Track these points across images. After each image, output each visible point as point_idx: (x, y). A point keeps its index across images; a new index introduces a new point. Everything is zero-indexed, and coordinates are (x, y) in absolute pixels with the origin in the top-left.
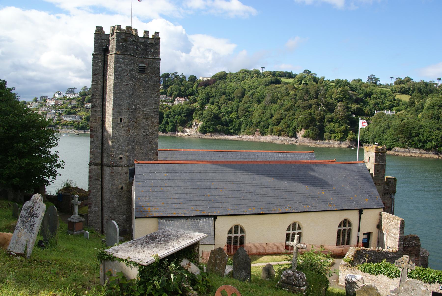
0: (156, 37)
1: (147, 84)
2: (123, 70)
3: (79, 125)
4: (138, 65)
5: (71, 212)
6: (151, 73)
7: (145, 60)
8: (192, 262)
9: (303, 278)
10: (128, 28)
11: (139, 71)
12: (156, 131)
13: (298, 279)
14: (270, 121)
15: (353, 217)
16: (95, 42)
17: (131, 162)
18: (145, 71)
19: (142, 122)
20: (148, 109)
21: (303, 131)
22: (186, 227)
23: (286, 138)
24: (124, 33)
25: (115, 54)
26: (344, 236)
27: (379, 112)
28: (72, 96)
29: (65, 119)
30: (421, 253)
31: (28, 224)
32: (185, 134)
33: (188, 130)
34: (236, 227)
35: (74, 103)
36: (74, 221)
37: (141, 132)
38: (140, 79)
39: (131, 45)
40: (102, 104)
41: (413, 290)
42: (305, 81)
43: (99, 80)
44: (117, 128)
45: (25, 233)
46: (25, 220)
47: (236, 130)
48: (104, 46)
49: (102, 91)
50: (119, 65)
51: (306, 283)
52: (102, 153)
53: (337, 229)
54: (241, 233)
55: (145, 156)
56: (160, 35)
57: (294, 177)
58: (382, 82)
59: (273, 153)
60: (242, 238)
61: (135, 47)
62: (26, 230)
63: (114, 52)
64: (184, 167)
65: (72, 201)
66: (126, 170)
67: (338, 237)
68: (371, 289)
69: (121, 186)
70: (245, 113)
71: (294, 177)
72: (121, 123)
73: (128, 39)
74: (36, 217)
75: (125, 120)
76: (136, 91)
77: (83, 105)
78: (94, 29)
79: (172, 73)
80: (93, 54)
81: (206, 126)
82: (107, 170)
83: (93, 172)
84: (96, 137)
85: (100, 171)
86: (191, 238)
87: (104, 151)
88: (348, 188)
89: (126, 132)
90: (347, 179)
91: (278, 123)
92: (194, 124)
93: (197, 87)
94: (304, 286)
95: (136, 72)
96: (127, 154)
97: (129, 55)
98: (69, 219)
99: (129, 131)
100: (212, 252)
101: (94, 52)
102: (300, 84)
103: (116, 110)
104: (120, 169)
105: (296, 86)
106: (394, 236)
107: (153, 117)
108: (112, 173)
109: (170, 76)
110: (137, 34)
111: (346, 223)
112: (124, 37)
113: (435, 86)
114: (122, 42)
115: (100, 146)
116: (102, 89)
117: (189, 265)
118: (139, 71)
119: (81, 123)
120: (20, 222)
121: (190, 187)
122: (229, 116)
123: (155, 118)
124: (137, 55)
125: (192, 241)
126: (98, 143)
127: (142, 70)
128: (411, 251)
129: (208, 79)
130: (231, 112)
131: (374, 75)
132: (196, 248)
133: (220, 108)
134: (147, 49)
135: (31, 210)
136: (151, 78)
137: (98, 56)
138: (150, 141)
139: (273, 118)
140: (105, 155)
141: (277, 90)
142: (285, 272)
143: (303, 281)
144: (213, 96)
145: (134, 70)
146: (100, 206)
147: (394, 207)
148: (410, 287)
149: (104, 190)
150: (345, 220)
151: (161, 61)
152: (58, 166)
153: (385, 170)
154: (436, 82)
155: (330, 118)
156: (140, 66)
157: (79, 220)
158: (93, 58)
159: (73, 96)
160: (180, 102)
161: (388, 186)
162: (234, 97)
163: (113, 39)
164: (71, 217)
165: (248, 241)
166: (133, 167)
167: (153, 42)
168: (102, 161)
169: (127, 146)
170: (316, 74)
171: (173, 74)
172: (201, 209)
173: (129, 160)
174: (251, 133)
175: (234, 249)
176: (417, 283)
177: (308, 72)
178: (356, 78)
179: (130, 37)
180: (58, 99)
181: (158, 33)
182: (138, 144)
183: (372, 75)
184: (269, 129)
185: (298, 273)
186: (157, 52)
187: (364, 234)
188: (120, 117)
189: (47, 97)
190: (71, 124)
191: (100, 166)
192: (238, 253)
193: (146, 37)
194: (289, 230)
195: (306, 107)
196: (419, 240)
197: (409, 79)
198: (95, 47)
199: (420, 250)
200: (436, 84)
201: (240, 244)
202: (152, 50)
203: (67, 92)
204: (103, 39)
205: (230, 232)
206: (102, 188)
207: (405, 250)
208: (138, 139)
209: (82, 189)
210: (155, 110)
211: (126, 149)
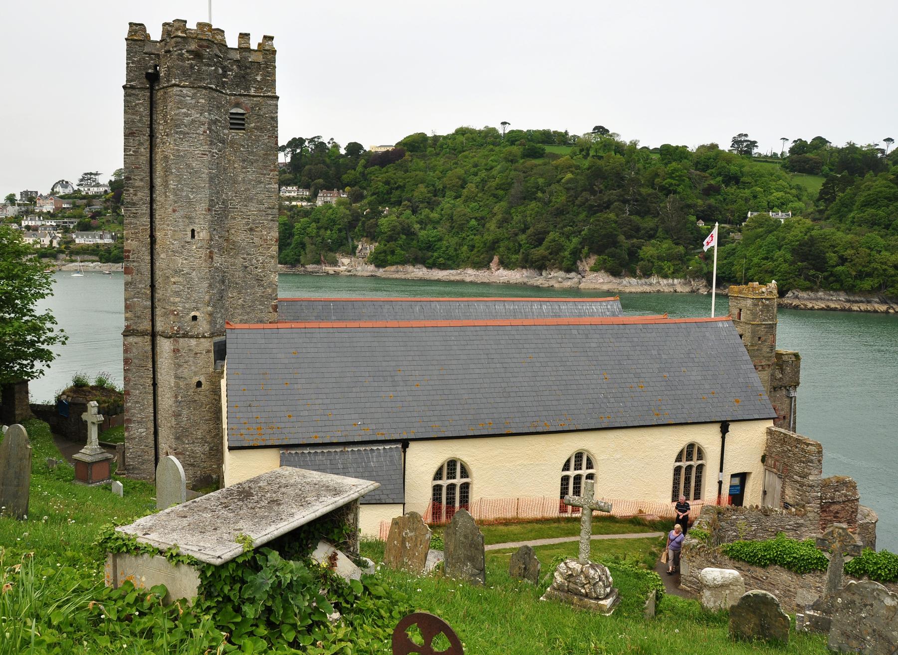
0: (267, 48)
1: (249, 153)
2: (193, 121)
4: (227, 111)
5: (82, 440)
6: (256, 128)
7: (243, 99)
9: (604, 577)
10: (200, 25)
11: (231, 124)
13: (593, 582)
14: (522, 238)
15: (707, 438)
16: (128, 59)
17: (218, 326)
18: (243, 125)
19: (241, 237)
20: (253, 207)
21: (593, 260)
22: (340, 466)
24: (193, 38)
26: (688, 480)
27: (755, 214)
28: (93, 190)
29: (77, 241)
30: (859, 516)
32: (343, 268)
33: (346, 261)
34: (452, 464)
35: (97, 206)
36: (88, 459)
37: (239, 261)
38: (232, 143)
39: (210, 66)
40: (148, 199)
41: (865, 605)
43: (140, 144)
44: (185, 252)
48: (150, 68)
49: (148, 171)
50: (184, 110)
51: (611, 591)
52: (153, 308)
53: (672, 464)
54: (462, 477)
55: (248, 313)
56: (276, 44)
57: (578, 354)
58: (762, 149)
59: (529, 304)
60: (465, 487)
61: (220, 71)
65: (84, 416)
66: (208, 344)
67: (674, 483)
68: (764, 603)
69: (196, 379)
71: (578, 354)
72: (193, 241)
73: (204, 52)
75: (202, 235)
76: (225, 170)
78: (125, 31)
79: (310, 137)
80: (124, 87)
81: (385, 252)
82: (165, 346)
83: (134, 350)
84: (139, 272)
85: (149, 348)
86: (336, 492)
87: (157, 304)
89: (206, 261)
90: (693, 356)
94: (607, 596)
95: (224, 128)
96: (210, 308)
97: (205, 88)
98: (76, 456)
99: (212, 258)
100: (395, 522)
102: (585, 157)
103: (182, 213)
104: (193, 342)
106: (799, 479)
107: (264, 227)
108: (176, 351)
109: (306, 143)
111: (691, 451)
112: (193, 46)
113: (879, 155)
114: (189, 59)
115: (149, 292)
116: (148, 166)
117: (333, 559)
118: (231, 119)
123: (270, 228)
124: (224, 88)
125: (341, 500)
126: (144, 286)
127: (237, 123)
128: (837, 513)
131: (746, 135)
132: (351, 517)
134: (248, 74)
136: (257, 141)
137: (136, 92)
138: (259, 280)
139: (529, 232)
140: (159, 311)
142: (562, 564)
143: (606, 587)
145: (220, 122)
146: (151, 425)
147: (795, 418)
148: (856, 598)
149: (160, 390)
150: (691, 446)
151: (280, 103)
153: (774, 336)
154: (883, 145)
155: (651, 229)
157: (100, 457)
158: (126, 95)
159: (96, 189)
161: (782, 370)
164: (82, 451)
165: (475, 496)
166: (223, 338)
167: (259, 58)
168: (153, 326)
169: (207, 292)
171: (311, 140)
173: (212, 322)
175: (447, 513)
176: (874, 590)
177: (600, 130)
178: (707, 142)
179: (208, 47)
180: (62, 197)
181: (272, 38)
182: (234, 288)
183: (740, 135)
185: (592, 566)
186: (270, 81)
187: (733, 476)
188: (191, 227)
189: (36, 192)
191: (148, 338)
192: (455, 523)
193: (244, 49)
194: (568, 470)
195: (598, 206)
196: (855, 487)
198: (129, 70)
199: (857, 509)
200: (883, 151)
201: (461, 502)
202: (259, 78)
203: (81, 180)
204: (146, 53)
205: (438, 475)
206: (155, 385)
207: (825, 511)
208: (233, 276)
210: (269, 211)
211: (207, 298)
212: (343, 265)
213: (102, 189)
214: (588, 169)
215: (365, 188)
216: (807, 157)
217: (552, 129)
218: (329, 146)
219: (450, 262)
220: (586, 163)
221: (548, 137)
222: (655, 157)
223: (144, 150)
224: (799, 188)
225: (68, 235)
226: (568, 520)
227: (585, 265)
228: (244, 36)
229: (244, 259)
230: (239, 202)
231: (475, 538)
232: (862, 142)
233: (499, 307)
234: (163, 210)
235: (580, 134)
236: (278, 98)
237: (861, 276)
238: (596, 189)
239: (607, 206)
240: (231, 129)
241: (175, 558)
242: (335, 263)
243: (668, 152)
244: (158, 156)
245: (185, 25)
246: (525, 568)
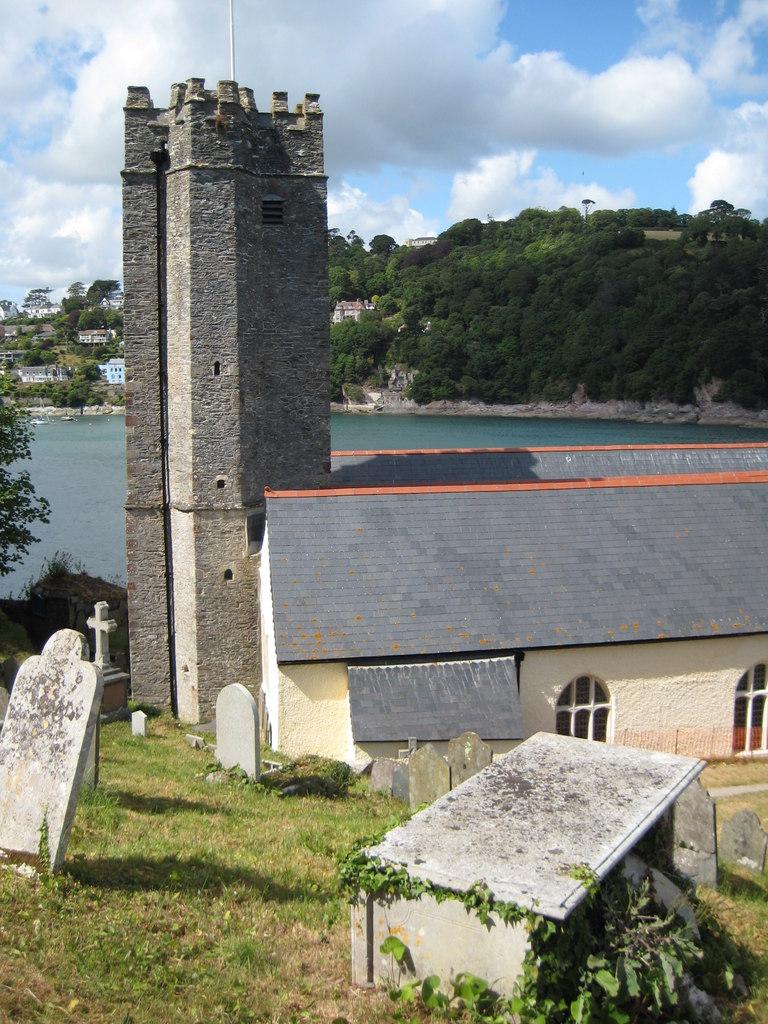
3: (66, 394)
7: (280, 182)
8: (655, 866)
11: (265, 216)
12: (322, 397)
18: (280, 217)
21: (716, 387)
23: (664, 408)
25: (189, 168)
28: (43, 312)
29: (25, 380)
31: (43, 743)
32: (371, 406)
33: (375, 396)
35: (49, 331)
42: (716, 236)
45: (34, 778)
46: (30, 727)
47: (514, 390)
61: (250, 145)
62: (36, 765)
63: (188, 163)
64: (416, 503)
69: (224, 568)
70: (540, 338)
74: (71, 717)
77: (73, 336)
81: (428, 382)
91: (640, 364)
92: (394, 376)
93: (398, 268)
101: (128, 165)
105: (689, 252)
107: (309, 356)
108: (198, 529)
110: (252, 103)
118: (265, 216)
119: (69, 387)
120: (10, 734)
121: (438, 565)
122: (494, 348)
126: (151, 439)
129: (428, 242)
130: (498, 339)
133: (466, 327)
135: (46, 690)
139: (626, 350)
141: (633, 265)
144: (445, 293)
152: (30, 514)
156: (265, 202)
159: (46, 311)
160: (350, 313)
162: (507, 292)
163: (182, 122)
167: (301, 124)
170: (747, 212)
172: (474, 632)
174: (563, 397)
184: (615, 383)
190: (44, 391)
202: (301, 152)
203: (28, 300)
209: (99, 580)
210: (318, 334)
212: (372, 401)
213: (54, 310)
214: (707, 260)
215: (398, 297)
217: (654, 207)
218: (350, 241)
219: (516, 394)
220: (704, 252)
223: (150, 258)
225: (13, 372)
226: (745, 761)
227: (705, 394)
228: (281, 96)
229: (285, 400)
230: (277, 323)
231: (703, 806)
233: (625, 458)
234: (176, 337)
238: (720, 287)
240: (264, 223)
241: (478, 901)
242: (361, 399)
244: (170, 263)
245: (202, 86)
246: (745, 843)
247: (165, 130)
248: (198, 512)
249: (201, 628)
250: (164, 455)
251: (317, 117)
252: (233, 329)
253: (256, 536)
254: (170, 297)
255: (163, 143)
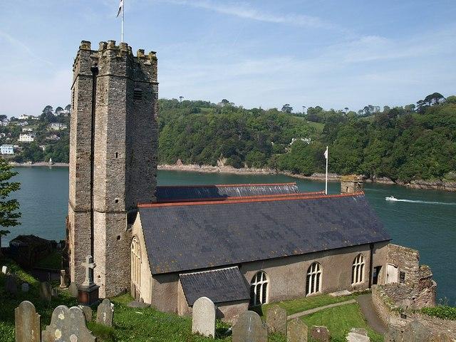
21: (225, 160)
25: (109, 75)
56: (157, 55)
88: (356, 221)
108: (107, 220)
140: (95, 198)
154: (344, 111)
167: (148, 62)
168: (92, 205)
177: (225, 101)
181: (155, 53)
197: (319, 109)
200: (345, 113)
206: (92, 239)
216: (315, 114)
217: (214, 97)
221: (201, 104)
222: (251, 113)
223: (89, 109)
224: (312, 128)
228: (142, 51)
232: (336, 109)
235: (216, 103)
236: (157, 84)
237: (343, 167)
239: (230, 136)
243: (256, 112)
247: (97, 59)
248: (108, 212)
249: (107, 259)
250: (92, 190)
251: (155, 59)
252: (123, 140)
253: (131, 220)
254: (96, 126)
255: (96, 64)
